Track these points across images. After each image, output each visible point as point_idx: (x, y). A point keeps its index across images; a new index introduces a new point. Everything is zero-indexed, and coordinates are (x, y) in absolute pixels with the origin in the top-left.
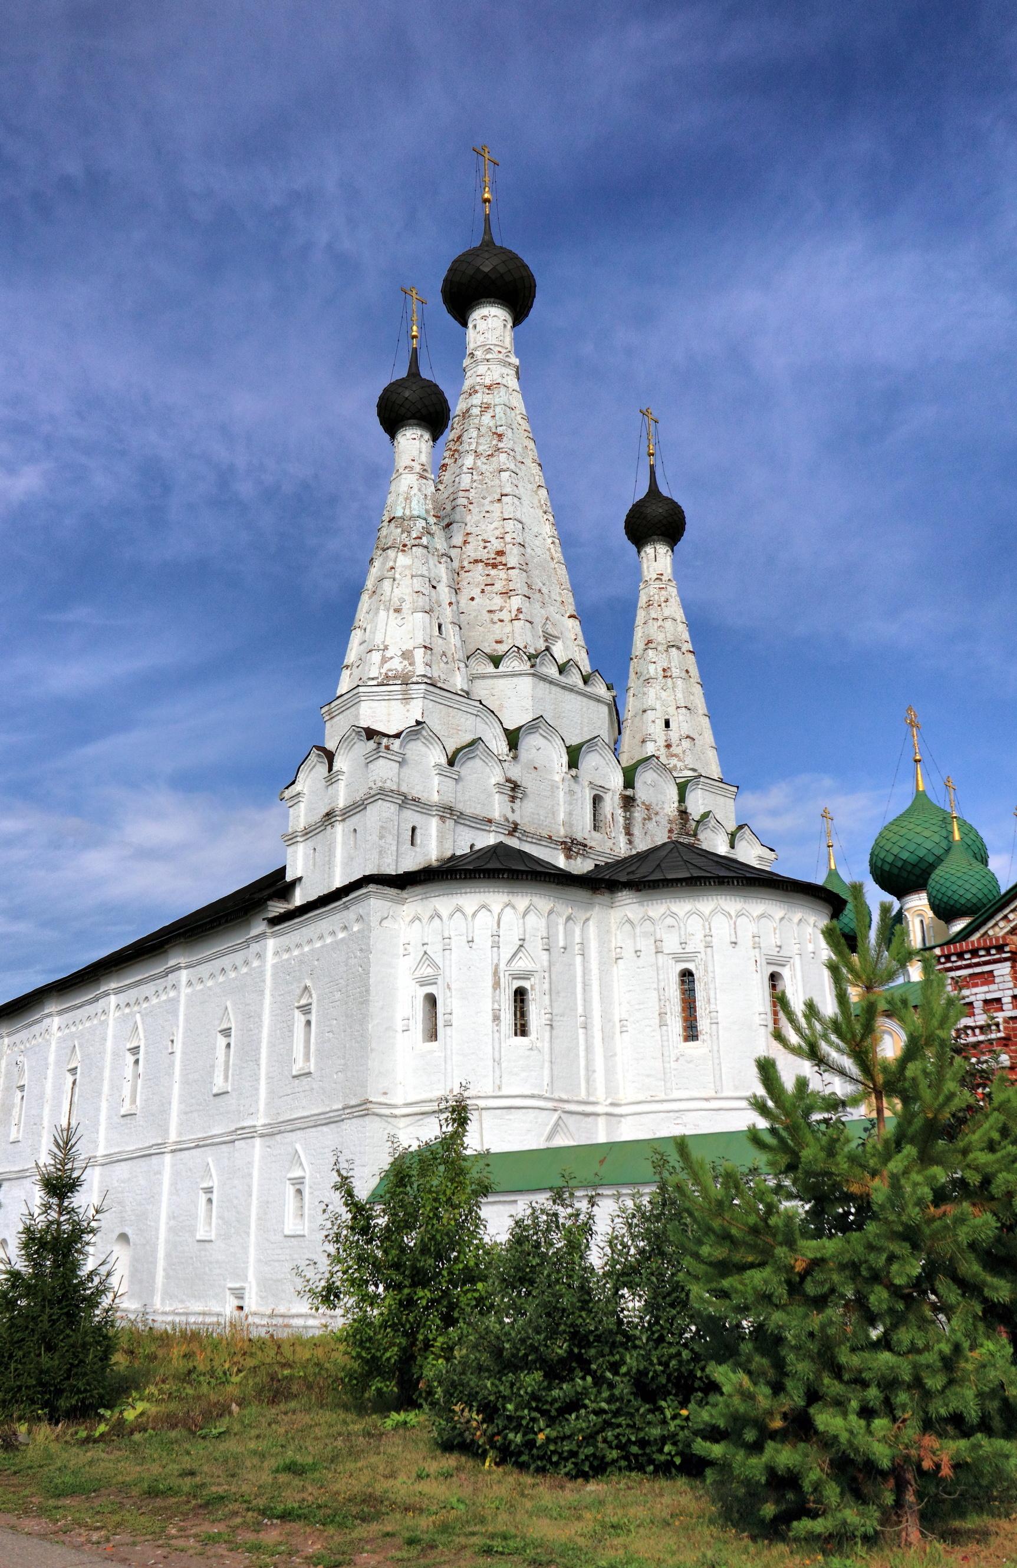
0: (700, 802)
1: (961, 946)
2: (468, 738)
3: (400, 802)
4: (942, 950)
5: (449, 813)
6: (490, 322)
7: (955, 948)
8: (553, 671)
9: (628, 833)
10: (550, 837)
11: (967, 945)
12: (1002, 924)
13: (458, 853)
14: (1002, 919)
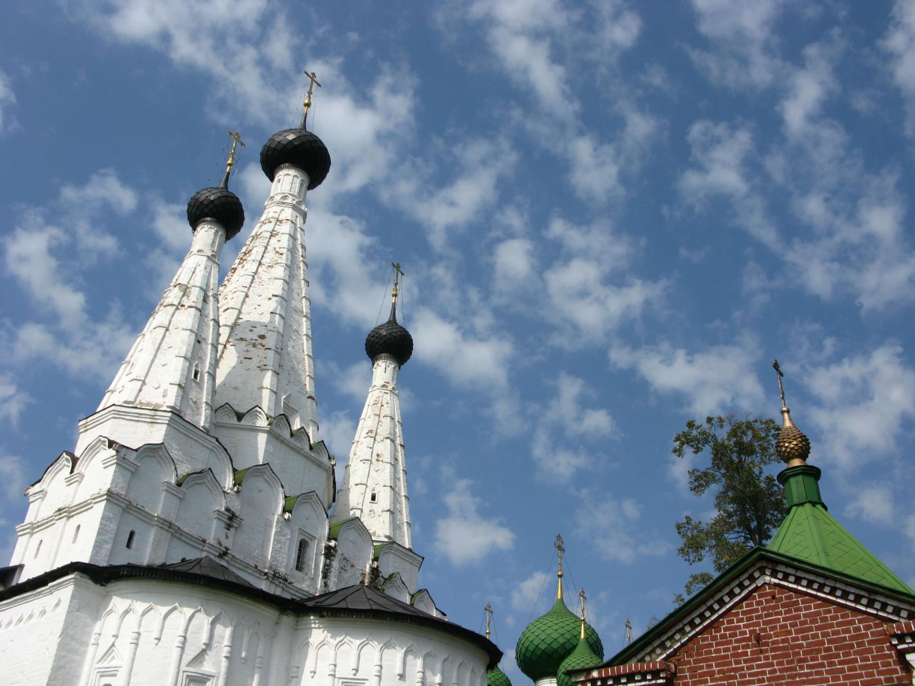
0: (391, 564)
1: (619, 670)
2: (199, 467)
3: (124, 506)
4: (600, 673)
5: (169, 527)
6: (288, 179)
7: (613, 671)
8: (286, 434)
9: (325, 575)
10: (256, 567)
11: (625, 669)
12: (658, 651)
13: (168, 563)
14: (659, 646)
